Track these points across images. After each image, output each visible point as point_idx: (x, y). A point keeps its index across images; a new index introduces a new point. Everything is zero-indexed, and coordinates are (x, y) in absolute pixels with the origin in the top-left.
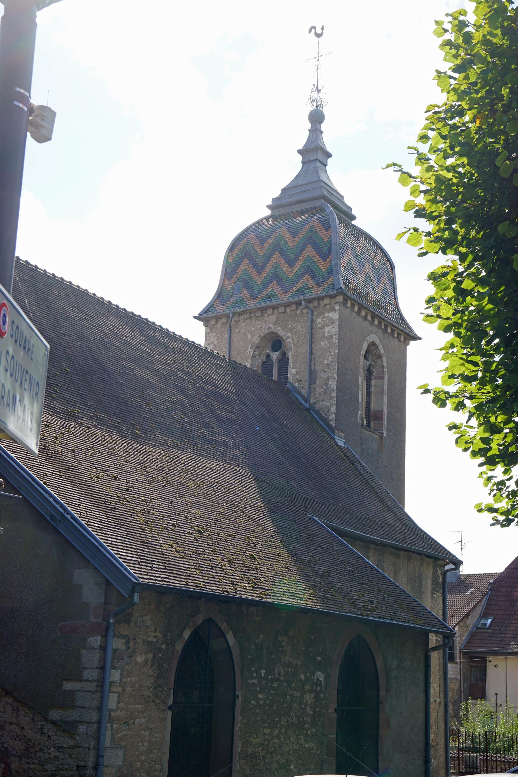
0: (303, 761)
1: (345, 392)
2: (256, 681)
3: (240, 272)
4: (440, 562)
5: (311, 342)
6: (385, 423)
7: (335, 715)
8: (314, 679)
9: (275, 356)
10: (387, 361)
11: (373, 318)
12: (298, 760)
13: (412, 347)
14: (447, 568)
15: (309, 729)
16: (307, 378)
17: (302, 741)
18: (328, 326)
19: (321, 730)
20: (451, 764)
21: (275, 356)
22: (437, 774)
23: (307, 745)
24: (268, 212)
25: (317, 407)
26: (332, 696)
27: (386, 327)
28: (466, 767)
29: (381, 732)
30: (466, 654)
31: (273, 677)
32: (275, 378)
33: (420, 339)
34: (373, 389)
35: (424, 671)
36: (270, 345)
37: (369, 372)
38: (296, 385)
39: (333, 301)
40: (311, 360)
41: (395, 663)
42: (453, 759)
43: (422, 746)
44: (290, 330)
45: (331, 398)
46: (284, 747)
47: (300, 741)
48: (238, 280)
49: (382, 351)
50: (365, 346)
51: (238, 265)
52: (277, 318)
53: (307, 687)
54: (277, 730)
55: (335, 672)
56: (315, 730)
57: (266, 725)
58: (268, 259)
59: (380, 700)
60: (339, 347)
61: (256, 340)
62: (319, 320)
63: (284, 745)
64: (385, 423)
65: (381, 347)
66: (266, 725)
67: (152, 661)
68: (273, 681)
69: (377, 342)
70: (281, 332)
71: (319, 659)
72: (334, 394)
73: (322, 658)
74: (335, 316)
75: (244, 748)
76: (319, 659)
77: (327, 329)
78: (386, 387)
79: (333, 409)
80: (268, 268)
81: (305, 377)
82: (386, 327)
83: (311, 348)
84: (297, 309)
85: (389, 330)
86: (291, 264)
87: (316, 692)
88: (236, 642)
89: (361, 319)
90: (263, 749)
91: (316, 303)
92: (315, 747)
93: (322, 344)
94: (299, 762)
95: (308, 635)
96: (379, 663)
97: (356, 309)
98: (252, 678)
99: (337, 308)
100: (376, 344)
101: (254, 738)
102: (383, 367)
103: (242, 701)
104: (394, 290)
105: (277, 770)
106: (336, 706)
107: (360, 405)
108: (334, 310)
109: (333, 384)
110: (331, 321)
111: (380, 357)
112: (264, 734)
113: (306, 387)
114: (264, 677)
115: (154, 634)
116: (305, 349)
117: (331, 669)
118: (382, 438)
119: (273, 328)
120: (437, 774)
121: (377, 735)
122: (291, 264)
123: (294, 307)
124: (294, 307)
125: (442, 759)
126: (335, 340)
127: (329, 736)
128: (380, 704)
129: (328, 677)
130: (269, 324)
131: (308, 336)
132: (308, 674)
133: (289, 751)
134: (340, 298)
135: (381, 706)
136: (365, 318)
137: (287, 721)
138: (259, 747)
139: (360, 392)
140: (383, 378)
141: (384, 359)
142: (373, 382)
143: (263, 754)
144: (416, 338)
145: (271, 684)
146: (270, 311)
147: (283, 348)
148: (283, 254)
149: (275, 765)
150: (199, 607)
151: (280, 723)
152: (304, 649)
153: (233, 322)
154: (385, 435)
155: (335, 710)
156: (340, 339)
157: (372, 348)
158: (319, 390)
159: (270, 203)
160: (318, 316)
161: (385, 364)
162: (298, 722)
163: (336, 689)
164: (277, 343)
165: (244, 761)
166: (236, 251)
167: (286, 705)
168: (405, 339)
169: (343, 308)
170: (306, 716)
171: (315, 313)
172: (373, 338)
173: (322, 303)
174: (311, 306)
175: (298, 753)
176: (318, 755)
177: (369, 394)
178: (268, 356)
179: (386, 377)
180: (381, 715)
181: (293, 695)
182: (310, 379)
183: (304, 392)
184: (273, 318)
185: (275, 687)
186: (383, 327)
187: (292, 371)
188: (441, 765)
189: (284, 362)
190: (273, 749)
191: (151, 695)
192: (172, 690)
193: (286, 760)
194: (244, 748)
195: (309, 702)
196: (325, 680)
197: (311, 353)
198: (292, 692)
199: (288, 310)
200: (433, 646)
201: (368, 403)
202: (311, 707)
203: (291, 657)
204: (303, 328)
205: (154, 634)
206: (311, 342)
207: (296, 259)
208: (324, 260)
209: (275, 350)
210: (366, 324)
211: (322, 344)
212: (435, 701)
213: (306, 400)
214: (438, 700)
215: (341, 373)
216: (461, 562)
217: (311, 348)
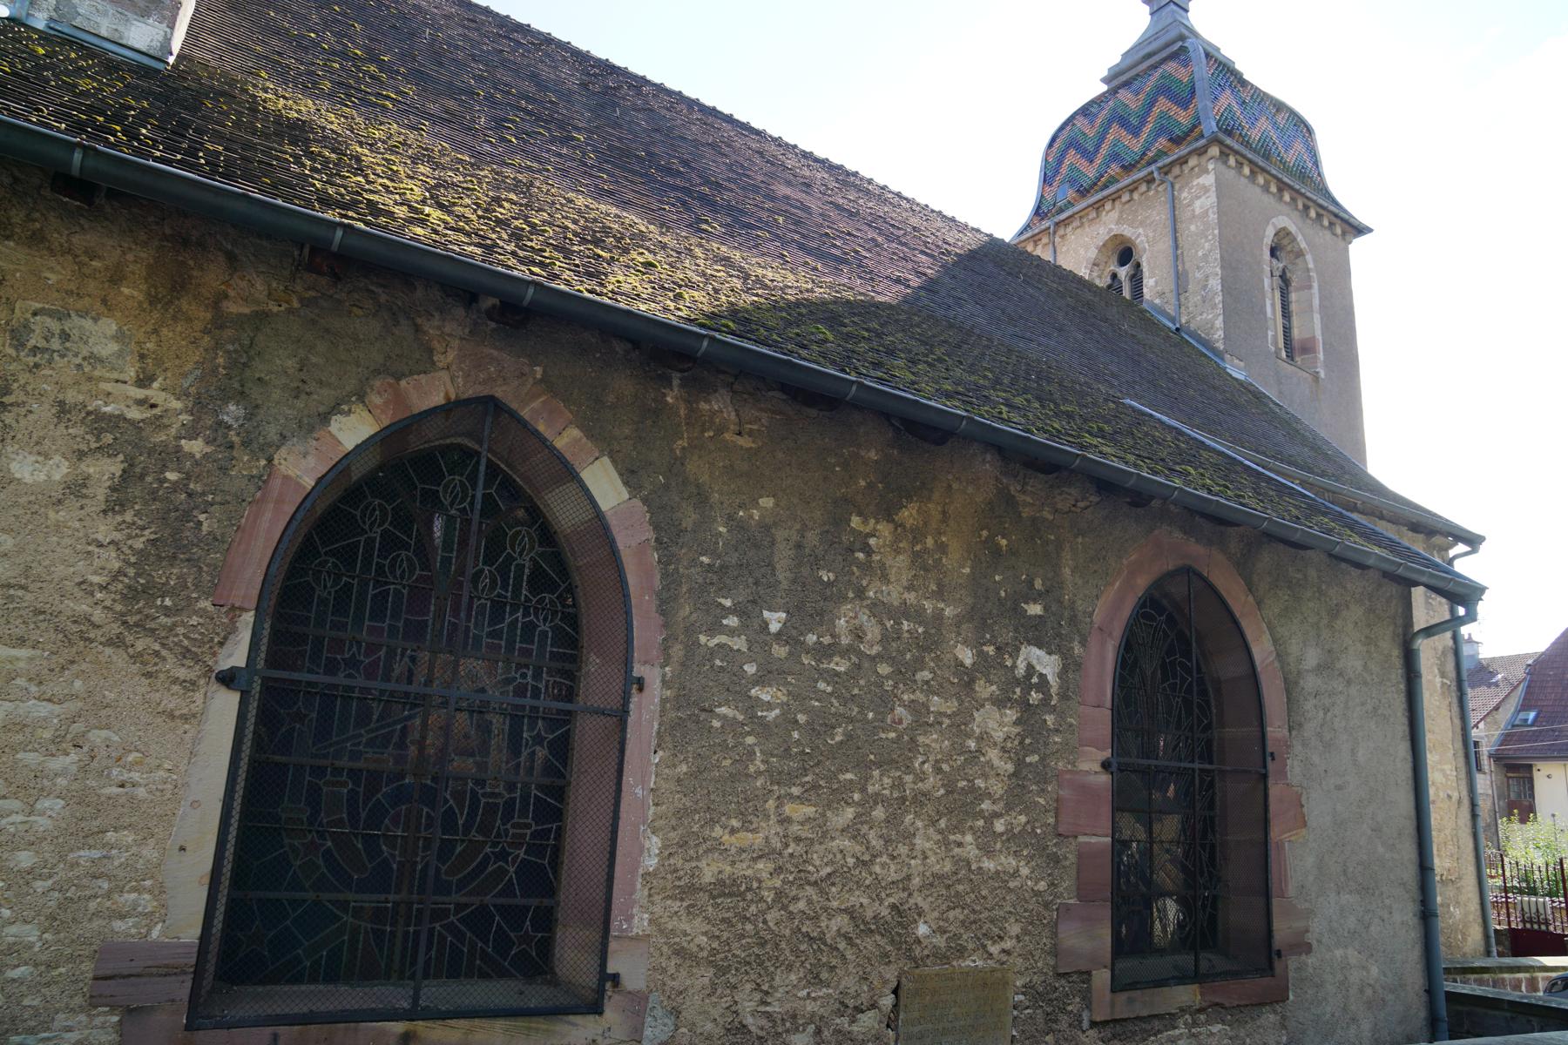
0: (974, 911)
1: (1238, 297)
2: (739, 643)
3: (1064, 170)
4: (1438, 540)
5: (1175, 231)
6: (1321, 356)
7: (1104, 779)
8: (1014, 666)
9: (1123, 272)
10: (1315, 261)
11: (1280, 190)
12: (949, 908)
13: (1358, 249)
14: (1452, 553)
15: (997, 815)
16: (1173, 287)
17: (971, 851)
18: (1198, 198)
19: (1051, 820)
20: (1492, 914)
21: (1123, 272)
22: (1463, 934)
23: (989, 865)
24: (1105, 88)
25: (1192, 326)
26: (1095, 717)
27: (1306, 208)
28: (1523, 921)
29: (1274, 833)
30: (1497, 757)
31: (827, 640)
32: (1127, 293)
33: (1370, 230)
34: (1293, 307)
35: (1402, 686)
36: (1115, 258)
37: (1285, 280)
38: (1157, 301)
39: (1204, 158)
40: (1176, 258)
41: (1312, 658)
42: (1496, 904)
43: (1410, 873)
44: (1142, 224)
45: (1214, 306)
46: (883, 865)
47: (957, 850)
48: (1062, 182)
49: (1303, 245)
50: (1270, 232)
51: (1060, 162)
52: (1121, 212)
53: (984, 689)
54: (850, 813)
55: (1102, 659)
56: (1023, 819)
57: (796, 791)
58: (1102, 137)
59: (1269, 749)
60: (1220, 225)
61: (1093, 253)
62: (1185, 194)
63: (885, 858)
64: (1321, 356)
65: (1300, 238)
66: (796, 791)
67: (113, 489)
68: (823, 652)
69: (1293, 229)
70: (1128, 231)
71: (1035, 609)
72: (1219, 299)
73: (1046, 609)
74: (1208, 180)
75: (677, 861)
76: (1035, 609)
77: (1198, 203)
78: (1316, 302)
79: (1219, 323)
80: (1104, 150)
81: (1168, 286)
82: (1306, 208)
83: (1176, 240)
84: (1149, 189)
85: (1313, 214)
86: (1136, 132)
87: (1025, 705)
88: (637, 502)
89: (1258, 190)
90: (779, 870)
91: (1176, 171)
92: (1025, 871)
93: (1193, 228)
94: (956, 913)
95: (985, 533)
96: (1262, 650)
97: (1246, 171)
98: (715, 628)
99: (1211, 167)
100: (1289, 233)
101: (733, 831)
102: (1308, 270)
103: (664, 701)
104: (1316, 164)
105: (849, 940)
106: (1107, 753)
107: (1270, 323)
108: (1207, 171)
109: (1215, 284)
110: (1204, 188)
111: (1300, 254)
112: (785, 821)
113: (1173, 301)
114: (779, 634)
115: (140, 393)
116: (1165, 244)
117: (1083, 643)
118: (1316, 376)
119: (1116, 229)
120: (1463, 934)
121: (1266, 842)
122: (1136, 132)
123: (1143, 188)
124: (1143, 188)
125: (1474, 906)
126: (1213, 217)
127: (1082, 839)
128: (1269, 759)
129: (1070, 666)
130: (1109, 224)
131: (1169, 223)
132: (990, 650)
133: (909, 878)
134: (1214, 151)
135: (1271, 766)
136: (1266, 188)
137: (898, 785)
138: (754, 860)
139: (1268, 303)
140: (1310, 287)
141: (1309, 257)
142: (1293, 296)
143: (778, 883)
144: (1360, 230)
145: (819, 661)
146: (1108, 206)
147: (1135, 257)
148: (1124, 123)
149: (841, 922)
150: (430, 351)
151: (863, 790)
152: (967, 570)
153: (1057, 239)
154: (1322, 375)
155: (1106, 765)
156: (1220, 213)
157: (1285, 242)
158: (1193, 298)
159: (1105, 73)
160: (1181, 189)
161: (1311, 266)
162: (948, 793)
163: (1108, 704)
164: (1126, 254)
165: (676, 905)
166: (1054, 149)
167: (892, 735)
168: (1344, 233)
169: (1221, 167)
170: (985, 776)
171: (1177, 187)
172: (1283, 221)
173: (1186, 168)
174: (1170, 178)
175: (948, 887)
176: (1037, 894)
177: (1286, 314)
178: (1114, 276)
179: (1315, 285)
180: (1274, 790)
181: (926, 706)
182: (1178, 286)
183: (1171, 310)
184: (1114, 215)
185: (837, 674)
186: (1300, 206)
187: (1149, 283)
188: (1471, 918)
189: (1137, 279)
190: (829, 870)
191: (98, 615)
192: (249, 617)
193: (893, 907)
194: (677, 861)
195: (999, 735)
196: (1063, 674)
197: (1177, 247)
198: (920, 697)
199: (1136, 196)
200: (1423, 626)
201: (1287, 331)
202: (1003, 749)
203: (910, 588)
204: (1158, 214)
205: (140, 393)
206: (1175, 231)
207: (1143, 122)
208: (1186, 109)
209: (1122, 263)
210: (1267, 199)
211: (1193, 228)
212: (1449, 797)
213: (1173, 320)
214: (1455, 795)
215: (1226, 264)
216: (1474, 620)
217: (1176, 240)
